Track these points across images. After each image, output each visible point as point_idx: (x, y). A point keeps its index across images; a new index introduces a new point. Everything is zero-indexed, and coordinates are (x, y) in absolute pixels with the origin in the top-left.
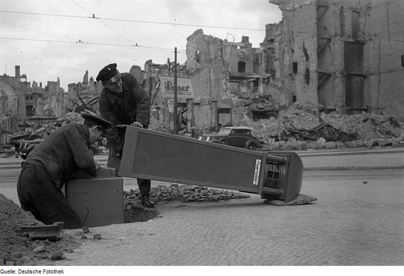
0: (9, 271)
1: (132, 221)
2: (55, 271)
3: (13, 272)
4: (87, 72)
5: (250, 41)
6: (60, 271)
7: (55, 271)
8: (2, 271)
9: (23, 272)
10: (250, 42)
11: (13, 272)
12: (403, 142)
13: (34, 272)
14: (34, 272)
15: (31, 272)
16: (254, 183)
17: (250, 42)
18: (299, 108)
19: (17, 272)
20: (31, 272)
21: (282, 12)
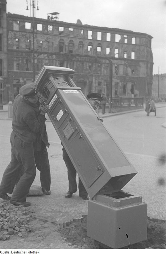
0: (5, 252)
1: (147, 36)
3: (8, 252)
6: (37, 252)
7: (34, 252)
8: (1, 252)
9: (14, 252)
11: (8, 252)
13: (21, 253)
14: (21, 253)
15: (19, 253)
19: (10, 252)
20: (19, 253)
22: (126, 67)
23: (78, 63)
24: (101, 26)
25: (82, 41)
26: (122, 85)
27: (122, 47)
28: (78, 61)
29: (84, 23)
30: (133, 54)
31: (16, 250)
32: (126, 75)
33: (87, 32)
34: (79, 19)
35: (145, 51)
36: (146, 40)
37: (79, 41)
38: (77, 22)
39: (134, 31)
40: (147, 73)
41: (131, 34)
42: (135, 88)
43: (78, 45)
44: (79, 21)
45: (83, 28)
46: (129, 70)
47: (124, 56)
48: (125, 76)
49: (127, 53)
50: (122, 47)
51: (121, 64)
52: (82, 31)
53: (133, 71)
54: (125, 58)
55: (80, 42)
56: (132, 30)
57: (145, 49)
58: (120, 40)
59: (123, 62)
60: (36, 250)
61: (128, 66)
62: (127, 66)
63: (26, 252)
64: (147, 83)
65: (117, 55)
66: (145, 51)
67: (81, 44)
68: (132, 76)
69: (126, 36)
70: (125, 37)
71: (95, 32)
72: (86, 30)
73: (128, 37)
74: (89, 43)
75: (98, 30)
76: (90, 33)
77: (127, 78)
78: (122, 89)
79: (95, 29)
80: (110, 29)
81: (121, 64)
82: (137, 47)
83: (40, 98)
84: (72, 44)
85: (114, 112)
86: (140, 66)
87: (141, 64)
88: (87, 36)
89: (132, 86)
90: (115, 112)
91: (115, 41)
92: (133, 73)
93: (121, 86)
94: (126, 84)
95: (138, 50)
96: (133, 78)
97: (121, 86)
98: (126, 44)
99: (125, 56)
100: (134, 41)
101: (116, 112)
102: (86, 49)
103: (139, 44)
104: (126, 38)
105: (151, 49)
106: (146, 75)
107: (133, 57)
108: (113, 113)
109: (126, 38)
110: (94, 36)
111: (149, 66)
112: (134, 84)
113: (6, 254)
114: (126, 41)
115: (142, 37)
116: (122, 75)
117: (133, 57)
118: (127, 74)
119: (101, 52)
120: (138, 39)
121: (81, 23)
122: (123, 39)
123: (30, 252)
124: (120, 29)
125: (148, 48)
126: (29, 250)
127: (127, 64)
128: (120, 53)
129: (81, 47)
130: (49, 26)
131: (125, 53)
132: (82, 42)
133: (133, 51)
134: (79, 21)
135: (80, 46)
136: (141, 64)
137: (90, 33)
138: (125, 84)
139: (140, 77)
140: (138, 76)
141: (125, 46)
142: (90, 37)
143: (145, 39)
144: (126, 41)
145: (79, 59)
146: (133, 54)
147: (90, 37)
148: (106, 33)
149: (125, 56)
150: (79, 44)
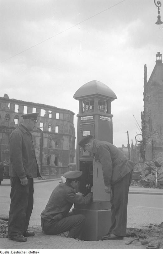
0: (5, 252)
1: (70, 113)
2: (34, 252)
3: (8, 252)
4: (145, 67)
5: (124, 146)
6: (37, 252)
7: (34, 252)
8: (1, 252)
9: (14, 252)
10: (112, 114)
11: (8, 252)
12: (162, 180)
13: (21, 253)
14: (21, 253)
15: (19, 253)
16: (92, 118)
17: (112, 114)
18: (159, 232)
19: (10, 252)
20: (19, 253)
21: (66, 181)
22: (50, 140)
23: (4, 134)
24: (27, 101)
25: (9, 114)
26: (46, 157)
27: (47, 121)
28: (4, 132)
29: (11, 97)
30: (57, 129)
31: (16, 250)
32: (50, 147)
33: (14, 106)
34: (6, 94)
35: (68, 126)
36: (69, 116)
37: (6, 113)
38: (4, 96)
39: (58, 107)
40: (70, 147)
41: (55, 110)
42: (58, 160)
43: (4, 118)
44: (6, 95)
45: (10, 102)
46: (53, 143)
47: (48, 129)
48: (49, 148)
49: (51, 127)
50: (47, 121)
51: (46, 137)
52: (9, 104)
53: (56, 144)
54: (50, 132)
55: (6, 115)
56: (56, 106)
57: (68, 124)
58: (45, 115)
59: (47, 135)
60: (36, 250)
61: (52, 139)
62: (51, 139)
63: (26, 252)
64: (69, 156)
65: (42, 128)
66: (68, 126)
67: (8, 117)
68: (56, 149)
69: (50, 112)
70: (49, 113)
71: (12, 105)
72: (13, 104)
73: (52, 112)
74: (15, 116)
75: (24, 104)
76: (17, 107)
77: (51, 151)
78: (47, 161)
79: (22, 104)
80: (36, 104)
81: (46, 137)
82: (61, 122)
83: (151, 140)
84: (8, 117)
85: (43, 179)
86: (63, 140)
87: (64, 137)
88: (14, 109)
89: (56, 158)
90: (45, 179)
91: (23, 112)
92: (56, 146)
93: (45, 157)
94: (50, 156)
95: (61, 124)
96: (57, 150)
97: (45, 157)
98: (50, 118)
99: (50, 130)
100: (57, 116)
101: (46, 179)
102: (12, 121)
103: (63, 119)
104: (50, 113)
105: (73, 124)
106: (69, 148)
107: (57, 131)
108: (43, 179)
109: (50, 113)
110: (21, 109)
111: (72, 140)
112: (58, 156)
113: (6, 254)
114: (50, 116)
115: (65, 113)
116: (46, 147)
117: (57, 131)
118: (51, 147)
119: (55, 126)
120: (62, 115)
121: (8, 97)
122: (47, 114)
123: (30, 252)
124: (46, 105)
125: (70, 124)
126: (29, 250)
127: (51, 137)
128: (45, 127)
129: (7, 119)
130: (24, 107)
131: (49, 127)
132: (9, 115)
133: (57, 126)
134: (6, 95)
135: (6, 118)
136: (64, 137)
137: (17, 107)
138: (49, 156)
139: (63, 150)
140: (61, 149)
141: (49, 120)
142: (16, 111)
143: (68, 115)
144: (50, 116)
145: (6, 131)
146: (57, 129)
147: (16, 111)
148: (40, 109)
149: (50, 130)
150: (6, 117)
